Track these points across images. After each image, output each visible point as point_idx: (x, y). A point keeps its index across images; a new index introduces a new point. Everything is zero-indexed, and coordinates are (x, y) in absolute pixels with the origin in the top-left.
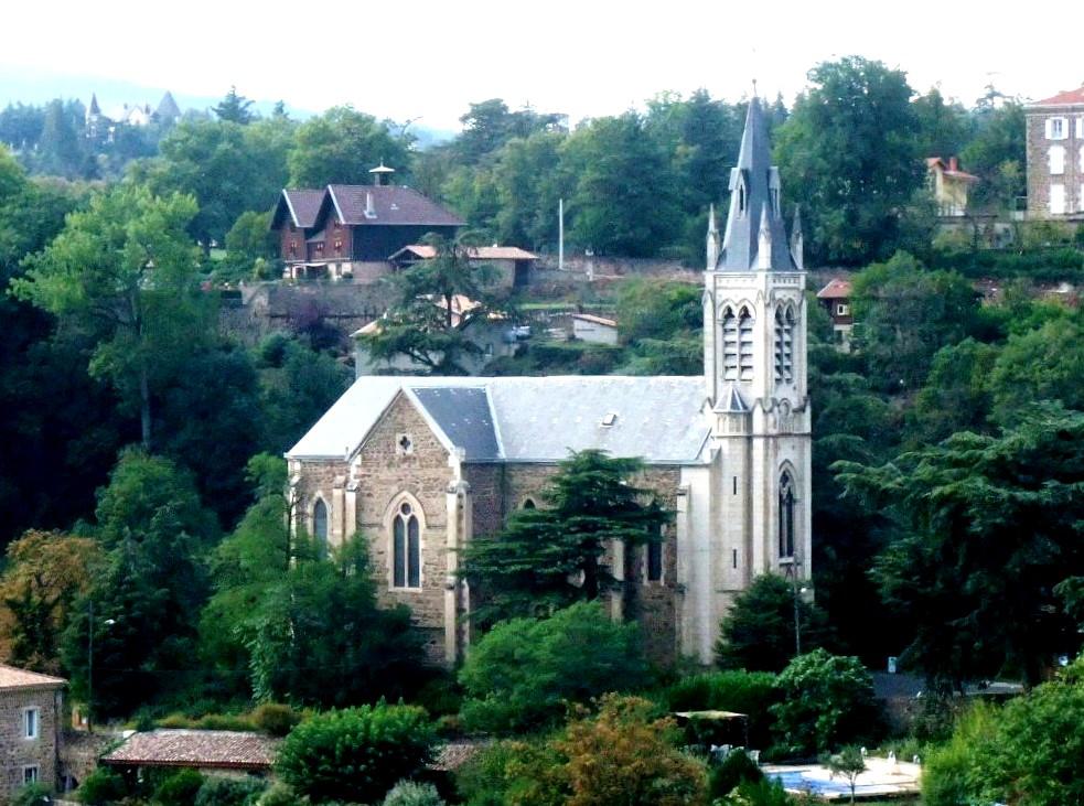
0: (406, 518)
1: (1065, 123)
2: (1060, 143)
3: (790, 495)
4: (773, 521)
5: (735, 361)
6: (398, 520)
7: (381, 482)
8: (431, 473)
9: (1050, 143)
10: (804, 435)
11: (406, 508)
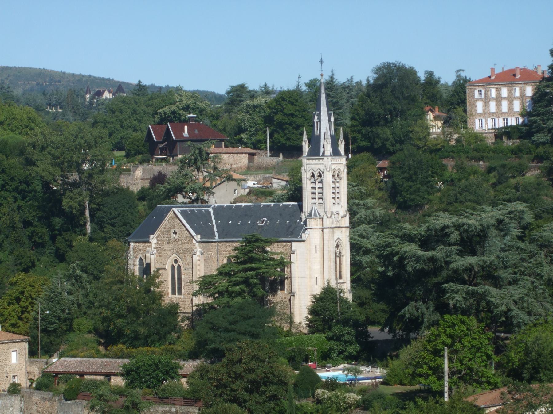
0: (176, 266)
1: (483, 91)
2: (481, 100)
3: (340, 253)
4: (333, 264)
5: (318, 196)
6: (173, 267)
7: (165, 250)
8: (187, 246)
9: (477, 100)
10: (347, 227)
11: (176, 261)
